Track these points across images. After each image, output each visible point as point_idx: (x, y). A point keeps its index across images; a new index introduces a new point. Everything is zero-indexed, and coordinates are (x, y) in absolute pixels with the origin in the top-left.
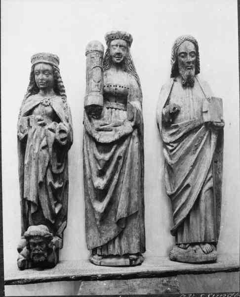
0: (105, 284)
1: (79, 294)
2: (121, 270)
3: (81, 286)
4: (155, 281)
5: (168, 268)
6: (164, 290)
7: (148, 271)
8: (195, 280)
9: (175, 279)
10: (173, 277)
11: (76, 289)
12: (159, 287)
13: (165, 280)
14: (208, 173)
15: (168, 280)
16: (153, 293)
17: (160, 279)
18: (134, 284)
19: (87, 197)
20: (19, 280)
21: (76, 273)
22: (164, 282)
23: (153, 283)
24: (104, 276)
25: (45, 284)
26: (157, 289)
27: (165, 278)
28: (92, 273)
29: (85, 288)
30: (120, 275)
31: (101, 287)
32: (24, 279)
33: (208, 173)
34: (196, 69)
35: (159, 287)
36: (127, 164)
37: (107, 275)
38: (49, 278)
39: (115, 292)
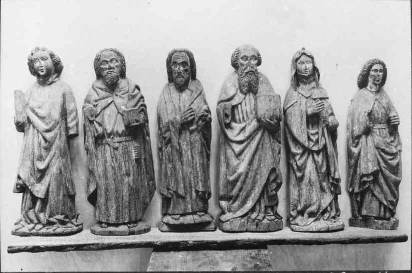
0: (180, 256)
1: (148, 270)
2: (198, 237)
3: (151, 258)
4: (242, 253)
5: (273, 236)
6: (253, 264)
7: (249, 239)
8: (286, 254)
9: (266, 252)
10: (262, 250)
11: (145, 261)
12: (247, 261)
13: (254, 252)
14: (88, 186)
15: (257, 253)
16: (240, 269)
17: (247, 252)
18: (216, 256)
19: (174, 164)
20: (93, 244)
21: (101, 240)
22: (252, 255)
23: (238, 256)
24: (196, 243)
25: (106, 252)
26: (245, 263)
27: (253, 250)
28: (182, 240)
29: (158, 260)
30: (216, 242)
31: (176, 260)
32: (98, 244)
33: (88, 186)
34: (371, 68)
35: (247, 261)
36: (281, 127)
37: (200, 241)
38: (130, 243)
39: (192, 267)
